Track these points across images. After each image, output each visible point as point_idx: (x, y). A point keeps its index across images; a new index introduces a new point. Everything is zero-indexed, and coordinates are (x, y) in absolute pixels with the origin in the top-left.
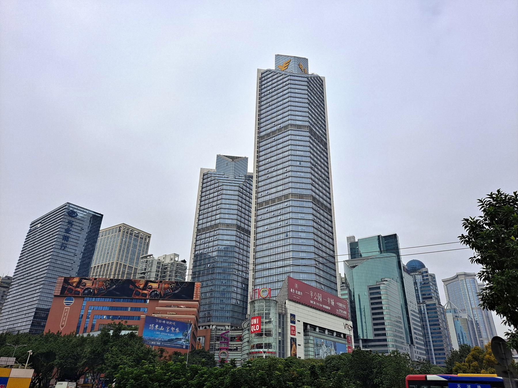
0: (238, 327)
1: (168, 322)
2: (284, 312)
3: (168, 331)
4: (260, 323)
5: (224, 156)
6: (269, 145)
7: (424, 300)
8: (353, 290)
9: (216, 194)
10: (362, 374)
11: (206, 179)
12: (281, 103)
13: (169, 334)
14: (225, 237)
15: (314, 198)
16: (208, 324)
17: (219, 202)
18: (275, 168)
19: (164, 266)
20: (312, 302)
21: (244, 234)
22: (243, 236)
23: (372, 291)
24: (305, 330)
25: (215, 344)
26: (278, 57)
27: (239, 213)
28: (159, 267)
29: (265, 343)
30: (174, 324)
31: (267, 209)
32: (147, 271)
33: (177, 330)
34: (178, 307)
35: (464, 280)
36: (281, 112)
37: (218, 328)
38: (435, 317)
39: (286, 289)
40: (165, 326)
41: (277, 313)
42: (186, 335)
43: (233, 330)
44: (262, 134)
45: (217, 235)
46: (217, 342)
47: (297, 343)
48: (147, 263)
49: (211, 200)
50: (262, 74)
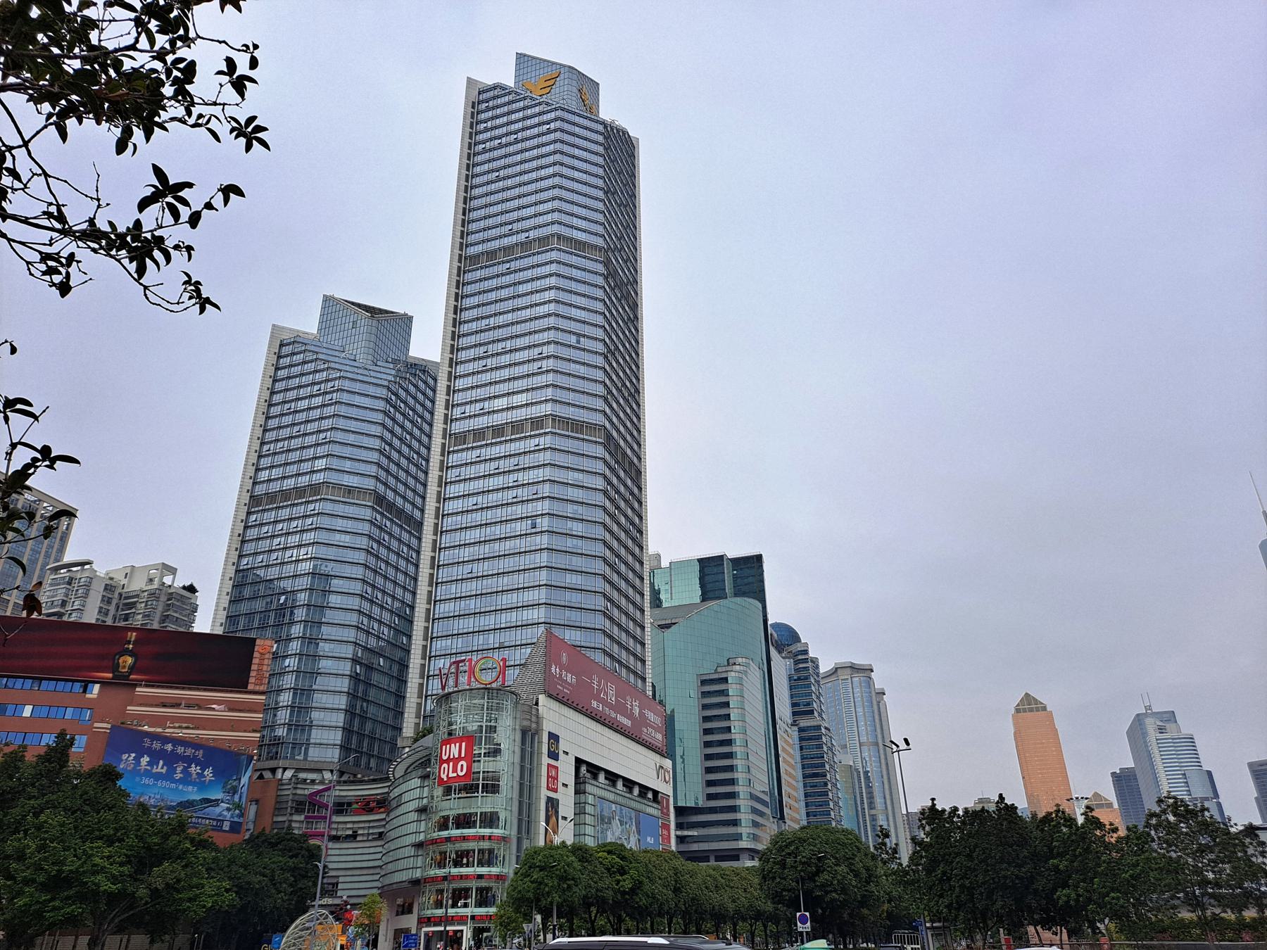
0: (359, 776)
1: (180, 750)
2: (534, 725)
3: (178, 776)
4: (471, 758)
5: (346, 301)
6: (493, 283)
7: (797, 718)
8: (662, 683)
9: (317, 401)
10: (1017, 877)
11: (287, 356)
12: (534, 175)
13: (181, 787)
14: (340, 524)
15: (609, 437)
16: (272, 764)
17: (326, 424)
18: (508, 345)
19: (126, 598)
20: (594, 704)
21: (391, 520)
22: (388, 524)
23: (707, 688)
24: (579, 781)
25: (291, 821)
26: (522, 58)
27: (384, 461)
28: (109, 601)
29: (481, 813)
30: (200, 756)
31: (479, 451)
32: (69, 608)
33: (208, 773)
34: (200, 708)
35: (850, 681)
36: (532, 199)
37: (302, 775)
38: (818, 758)
39: (540, 667)
40: (171, 759)
41: (517, 727)
42: (234, 791)
43: (345, 782)
44: (472, 251)
45: (314, 515)
46: (296, 818)
47: (561, 814)
48: (69, 583)
49: (301, 417)
50: (479, 94)
